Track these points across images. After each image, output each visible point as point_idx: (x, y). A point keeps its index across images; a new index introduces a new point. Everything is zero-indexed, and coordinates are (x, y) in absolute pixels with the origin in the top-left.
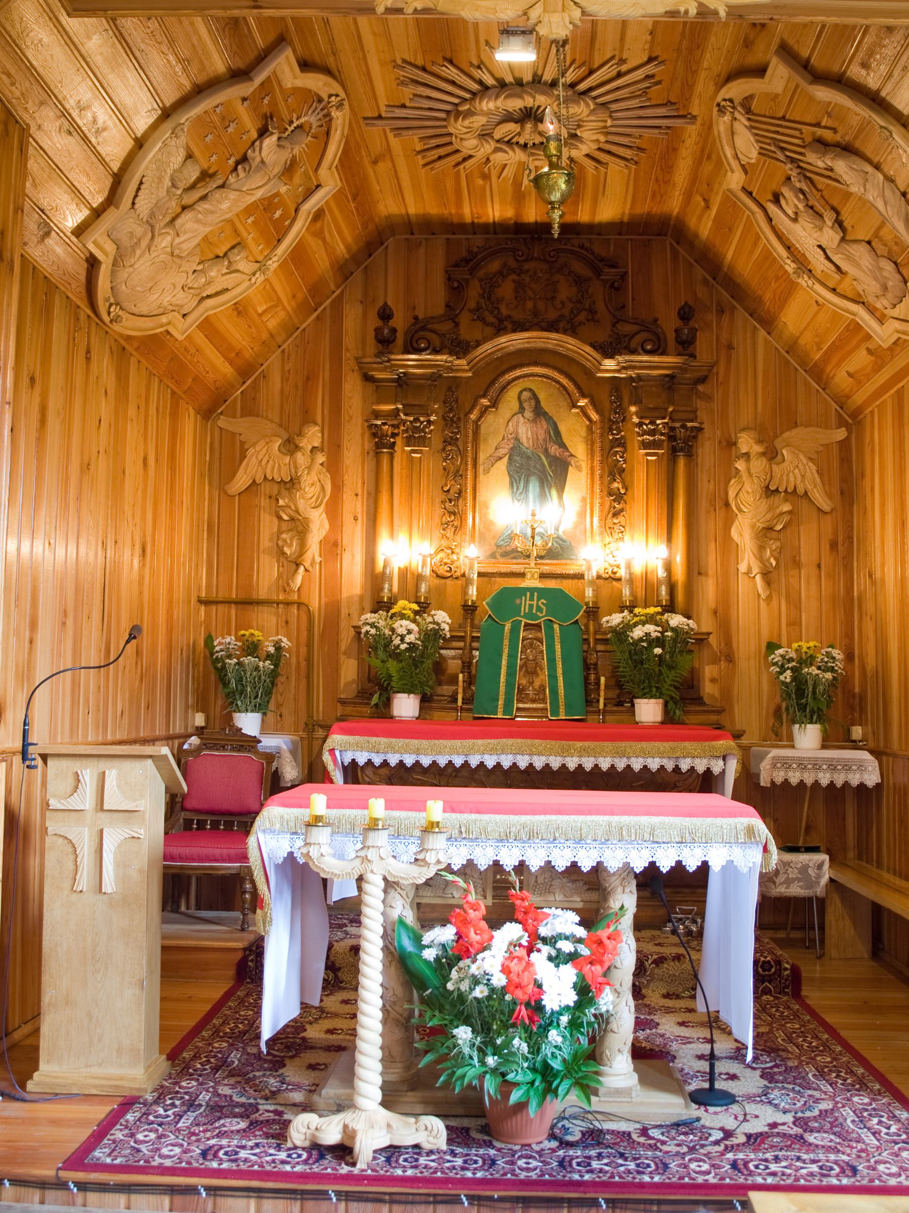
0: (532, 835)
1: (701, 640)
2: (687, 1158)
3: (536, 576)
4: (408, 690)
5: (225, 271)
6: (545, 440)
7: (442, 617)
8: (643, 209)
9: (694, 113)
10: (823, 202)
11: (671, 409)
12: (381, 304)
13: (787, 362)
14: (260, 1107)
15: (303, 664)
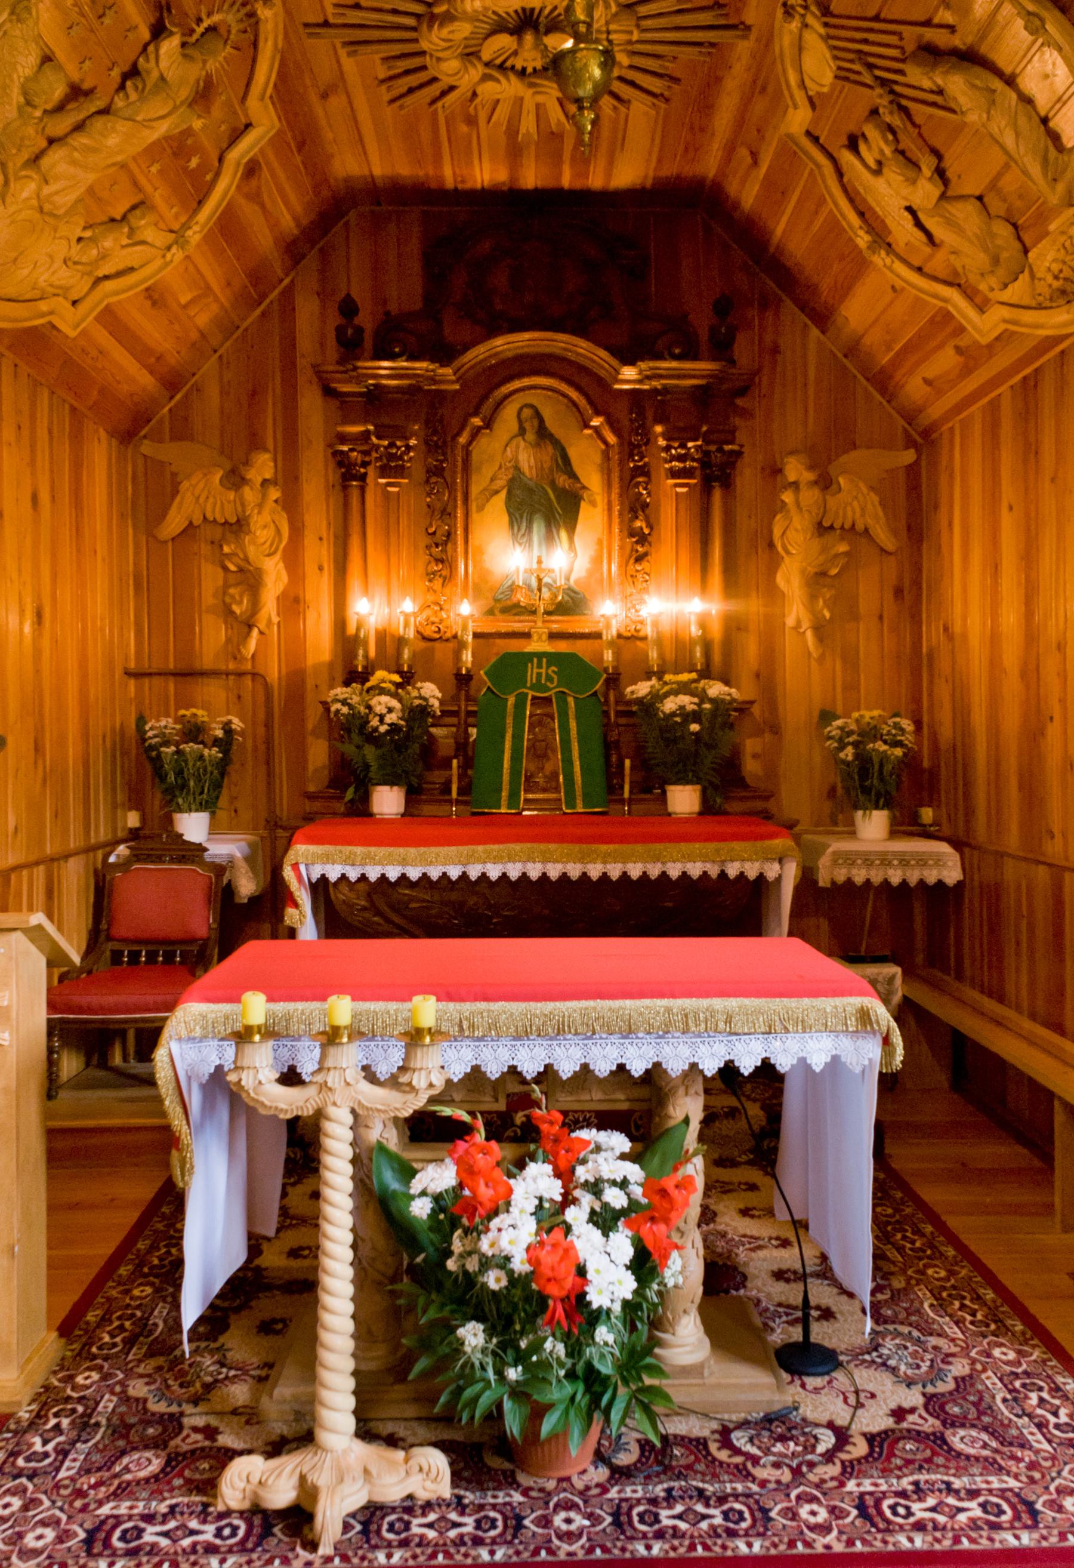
0: (560, 1030)
1: (743, 708)
2: (794, 1494)
3: (544, 637)
4: (391, 781)
5: (125, 241)
6: (551, 470)
7: (430, 691)
8: (669, 170)
9: (748, 22)
10: (920, 142)
11: (704, 428)
12: (343, 294)
13: (845, 367)
14: (186, 1421)
15: (262, 748)
